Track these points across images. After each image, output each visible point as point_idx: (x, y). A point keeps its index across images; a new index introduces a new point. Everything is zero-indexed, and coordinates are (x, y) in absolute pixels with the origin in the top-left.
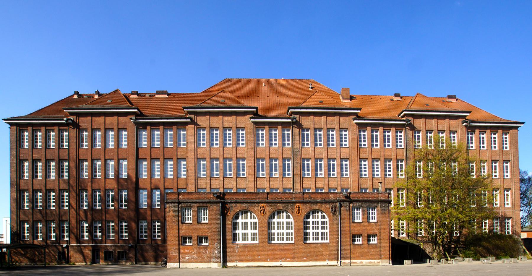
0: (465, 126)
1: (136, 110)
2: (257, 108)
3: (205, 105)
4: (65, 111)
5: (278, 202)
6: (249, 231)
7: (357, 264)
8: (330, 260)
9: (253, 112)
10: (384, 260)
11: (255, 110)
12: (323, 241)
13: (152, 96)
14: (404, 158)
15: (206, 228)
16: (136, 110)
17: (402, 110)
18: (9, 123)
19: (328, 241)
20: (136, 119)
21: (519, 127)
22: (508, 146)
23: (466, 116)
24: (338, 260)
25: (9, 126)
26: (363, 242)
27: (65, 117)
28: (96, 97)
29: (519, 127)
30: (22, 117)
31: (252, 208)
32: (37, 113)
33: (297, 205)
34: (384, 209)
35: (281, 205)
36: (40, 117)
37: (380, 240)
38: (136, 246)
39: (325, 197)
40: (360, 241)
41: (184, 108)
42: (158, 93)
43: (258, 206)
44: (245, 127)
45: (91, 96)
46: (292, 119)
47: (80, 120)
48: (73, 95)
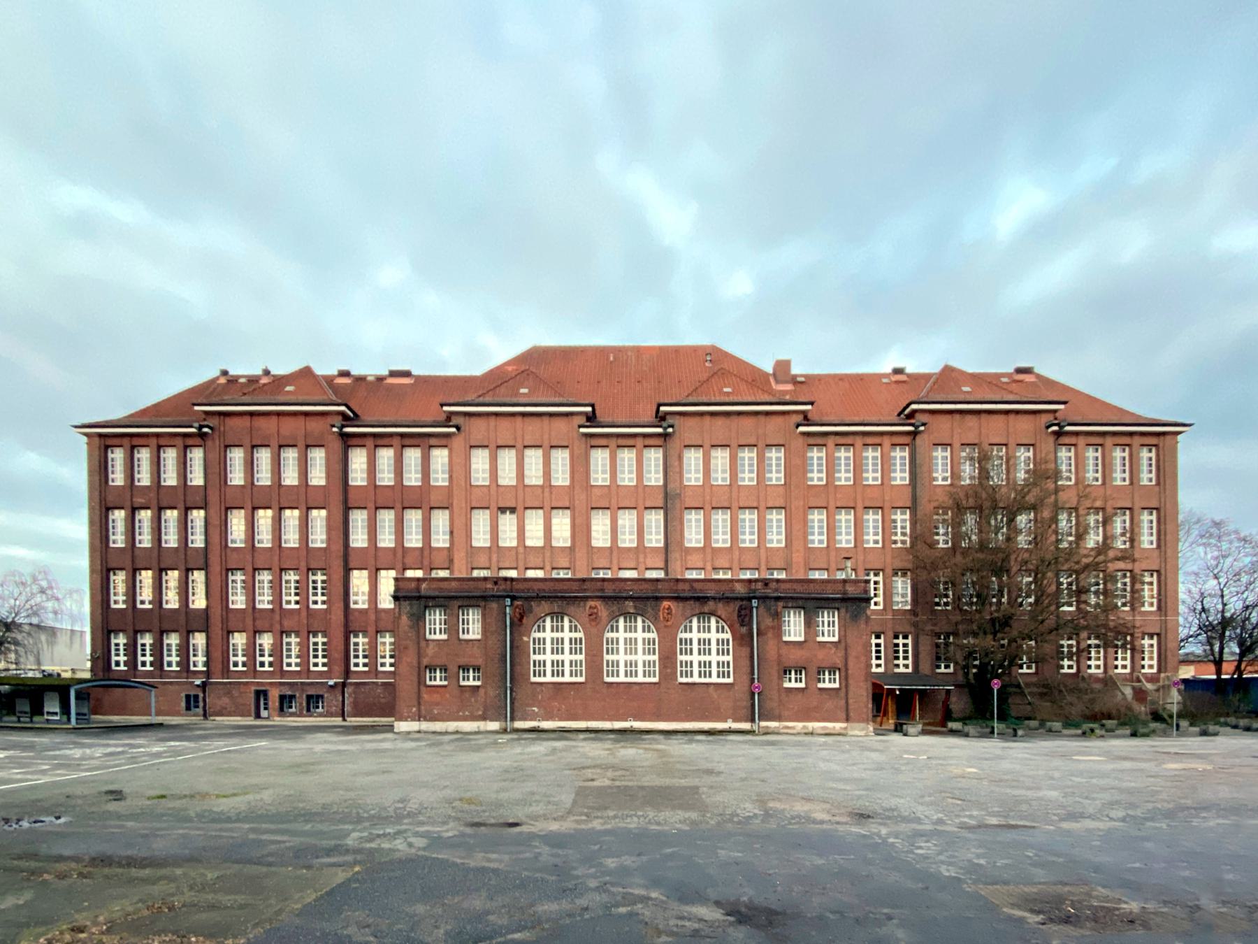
0: (1054, 433)
1: (343, 408)
2: (593, 406)
3: (488, 399)
4: (197, 408)
5: (626, 598)
6: (567, 657)
7: (794, 731)
8: (735, 720)
9: (586, 414)
10: (856, 725)
11: (589, 409)
12: (721, 680)
13: (380, 379)
14: (670, 577)
15: (476, 651)
16: (343, 408)
17: (907, 402)
18: (86, 434)
19: (730, 680)
20: (343, 426)
21: (1180, 433)
22: (1147, 477)
23: (1055, 411)
24: (753, 720)
25: (85, 439)
26: (955, 669)
27: (196, 421)
28: (264, 380)
29: (1180, 433)
30: (111, 421)
31: (572, 609)
32: (144, 412)
33: (666, 604)
34: (856, 616)
35: (631, 604)
36: (146, 420)
37: (845, 679)
38: (344, 685)
39: (724, 587)
40: (801, 681)
41: (442, 405)
42: (393, 374)
43: (585, 606)
44: (183, 695)
45: (253, 380)
46: (665, 429)
47: (227, 428)
48: (217, 378)
